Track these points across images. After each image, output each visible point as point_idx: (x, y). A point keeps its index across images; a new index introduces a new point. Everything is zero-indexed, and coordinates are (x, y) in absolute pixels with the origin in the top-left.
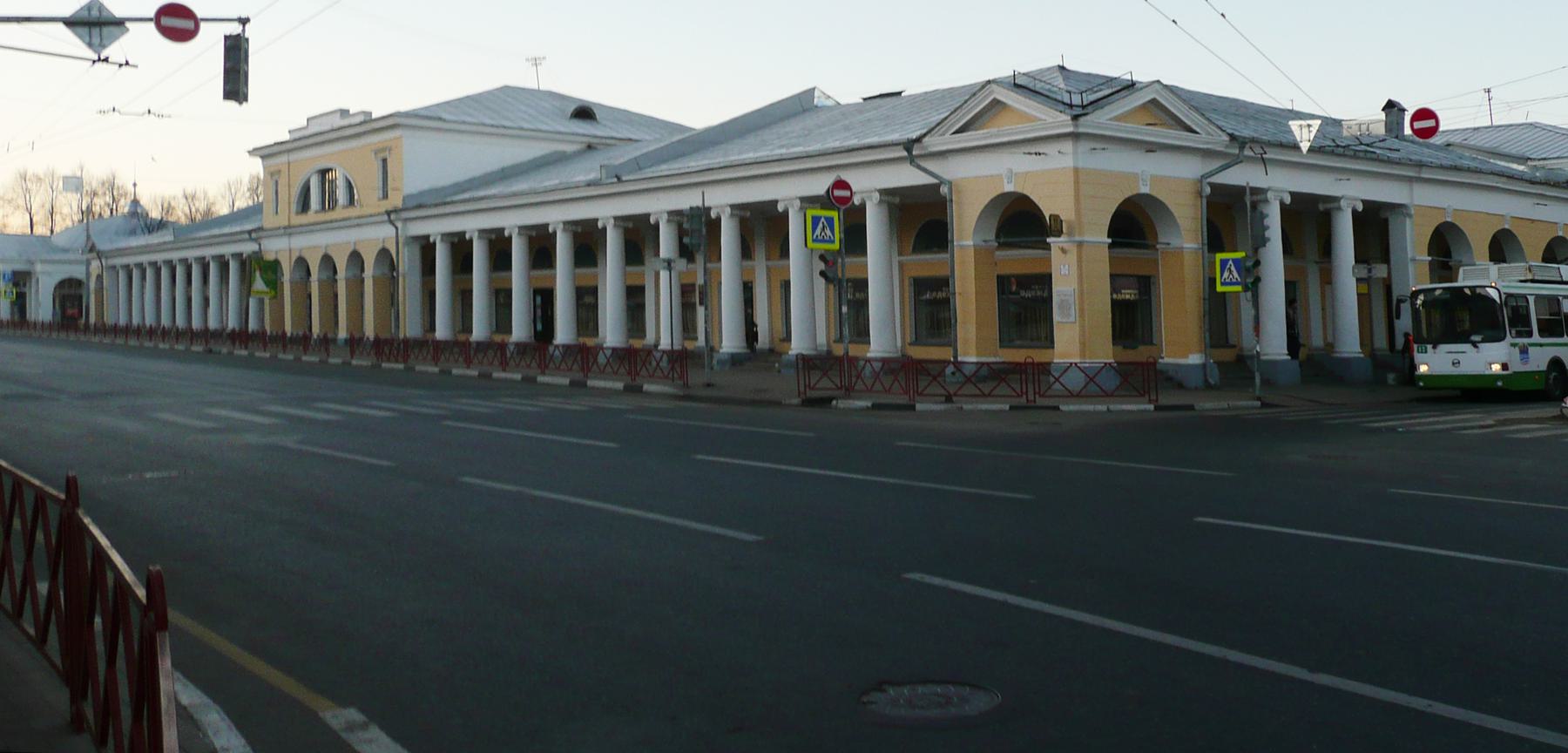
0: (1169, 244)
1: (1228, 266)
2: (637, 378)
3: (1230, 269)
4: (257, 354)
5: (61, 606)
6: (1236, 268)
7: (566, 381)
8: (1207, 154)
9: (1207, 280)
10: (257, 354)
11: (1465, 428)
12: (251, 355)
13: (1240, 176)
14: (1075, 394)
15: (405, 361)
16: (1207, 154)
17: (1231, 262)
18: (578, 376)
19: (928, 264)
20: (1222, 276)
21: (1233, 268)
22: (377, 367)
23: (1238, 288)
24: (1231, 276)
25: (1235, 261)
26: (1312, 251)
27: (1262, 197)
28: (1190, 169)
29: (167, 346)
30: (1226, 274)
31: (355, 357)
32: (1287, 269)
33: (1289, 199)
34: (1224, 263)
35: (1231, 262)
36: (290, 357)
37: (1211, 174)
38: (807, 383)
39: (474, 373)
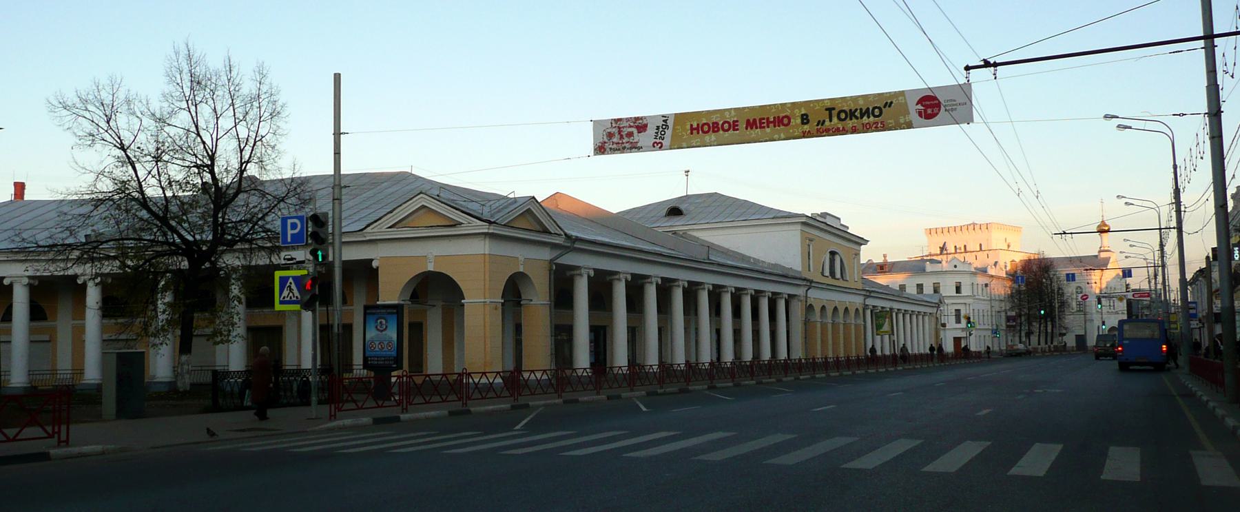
0: (531, 300)
1: (288, 284)
2: (519, 398)
3: (290, 286)
4: (845, 373)
5: (627, 453)
6: (297, 286)
7: (793, 378)
8: (554, 246)
9: (553, 326)
10: (845, 373)
11: (348, 447)
12: (841, 375)
13: (569, 259)
14: (11, 437)
15: (885, 367)
16: (554, 246)
17: (291, 280)
18: (457, 406)
19: (263, 318)
20: (281, 294)
21: (293, 286)
22: (813, 378)
23: (297, 307)
24: (291, 294)
25: (295, 278)
26: (692, 312)
27: (578, 272)
28: (545, 254)
29: (863, 372)
30: (286, 293)
31: (788, 375)
32: (629, 319)
33: (593, 273)
34: (284, 280)
35: (291, 280)
36: (863, 372)
37: (557, 258)
39: (850, 373)
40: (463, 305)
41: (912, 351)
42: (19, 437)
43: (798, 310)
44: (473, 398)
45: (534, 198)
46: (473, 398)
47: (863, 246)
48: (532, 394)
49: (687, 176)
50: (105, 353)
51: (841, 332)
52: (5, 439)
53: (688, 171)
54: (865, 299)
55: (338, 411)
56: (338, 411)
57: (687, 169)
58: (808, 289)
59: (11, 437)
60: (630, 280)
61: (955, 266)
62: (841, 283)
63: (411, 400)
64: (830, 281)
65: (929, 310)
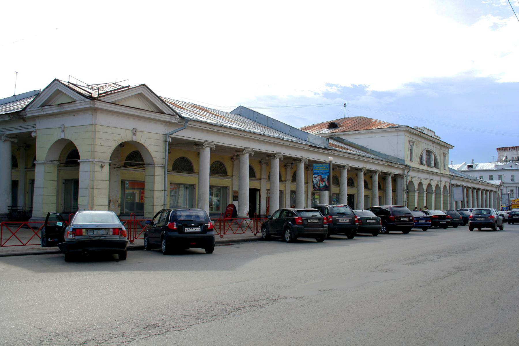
8: (168, 123)
14: (25, 244)
38: (135, 237)
40: (79, 163)
41: (507, 216)
42: (27, 244)
43: (402, 184)
44: (226, 234)
45: (144, 85)
46: (226, 234)
47: (450, 149)
48: (244, 233)
49: (345, 106)
50: (357, 208)
51: (442, 202)
52: (22, 244)
53: (345, 104)
54: (450, 181)
55: (136, 239)
56: (136, 239)
57: (345, 103)
58: (451, 180)
59: (25, 244)
60: (349, 170)
61: (511, 166)
62: (436, 170)
63: (225, 232)
64: (421, 167)
65: (494, 189)
